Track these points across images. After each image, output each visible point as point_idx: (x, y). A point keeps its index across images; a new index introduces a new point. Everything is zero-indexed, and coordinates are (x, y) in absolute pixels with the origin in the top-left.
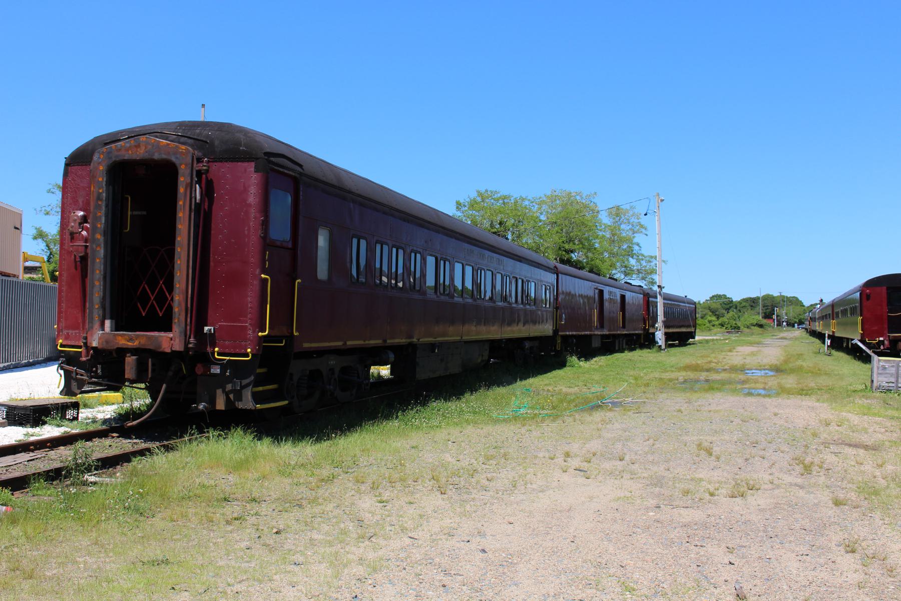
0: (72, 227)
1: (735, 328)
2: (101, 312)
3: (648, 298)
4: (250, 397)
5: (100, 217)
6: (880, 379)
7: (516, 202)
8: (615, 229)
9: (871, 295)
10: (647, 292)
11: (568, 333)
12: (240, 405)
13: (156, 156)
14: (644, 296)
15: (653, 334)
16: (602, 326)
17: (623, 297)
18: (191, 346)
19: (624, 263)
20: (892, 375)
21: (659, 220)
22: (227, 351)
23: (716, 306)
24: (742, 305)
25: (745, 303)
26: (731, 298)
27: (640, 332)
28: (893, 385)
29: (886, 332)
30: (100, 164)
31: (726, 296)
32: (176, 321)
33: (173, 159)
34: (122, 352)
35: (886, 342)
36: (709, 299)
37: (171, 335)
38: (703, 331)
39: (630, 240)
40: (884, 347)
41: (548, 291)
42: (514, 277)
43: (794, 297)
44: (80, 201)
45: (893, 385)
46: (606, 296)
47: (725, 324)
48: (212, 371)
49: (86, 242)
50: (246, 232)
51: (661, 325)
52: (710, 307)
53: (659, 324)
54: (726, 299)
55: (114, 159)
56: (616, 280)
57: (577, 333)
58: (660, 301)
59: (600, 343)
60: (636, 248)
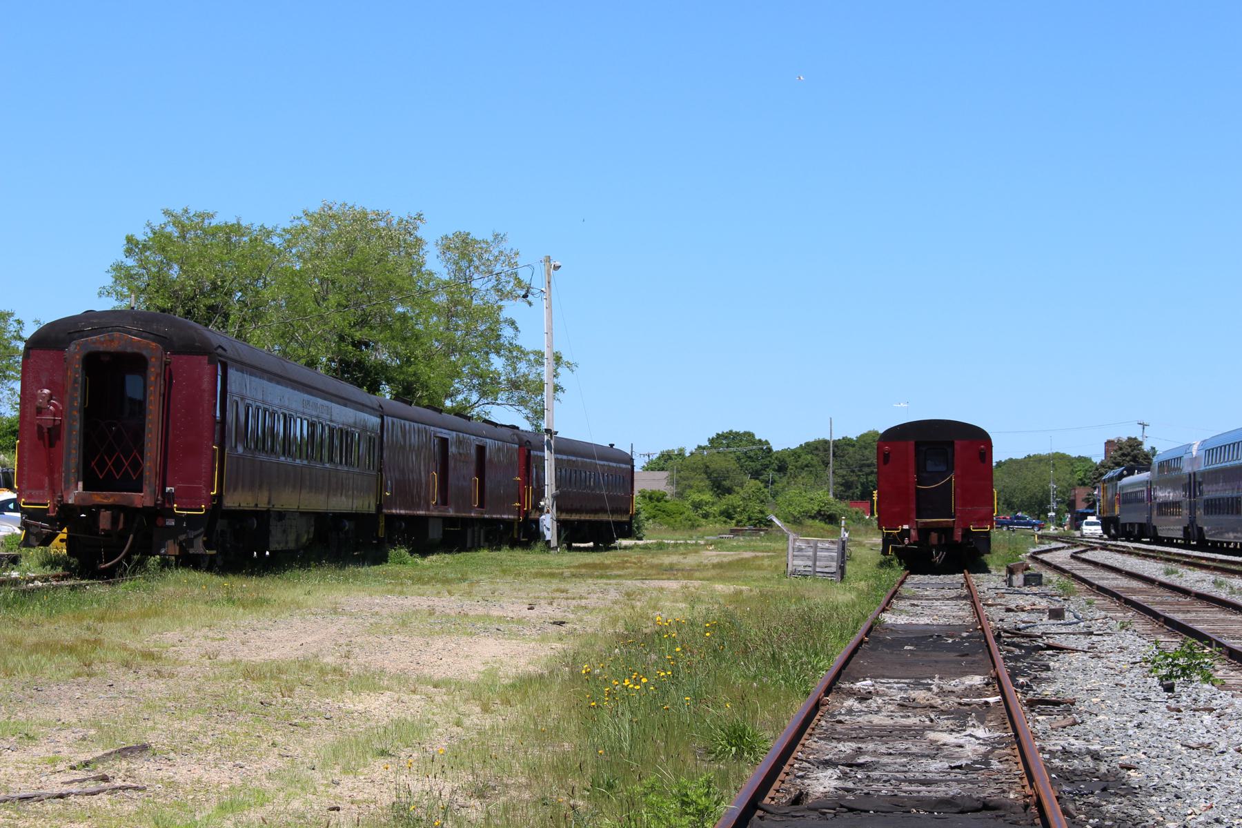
0: (41, 403)
1: (760, 522)
2: (76, 476)
3: (529, 451)
4: (201, 544)
5: (76, 397)
6: (796, 562)
7: (254, 241)
8: (460, 287)
9: (891, 455)
10: (525, 439)
11: (394, 511)
12: (191, 551)
13: (129, 350)
14: (520, 446)
15: (537, 522)
16: (444, 501)
17: (481, 450)
18: (159, 502)
19: (478, 368)
20: (808, 557)
21: (549, 307)
22: (184, 507)
23: (724, 464)
24: (802, 461)
25: (809, 457)
26: (767, 443)
27: (511, 517)
28: (810, 569)
29: (913, 515)
30: (75, 351)
31: (753, 435)
32: (147, 482)
33: (145, 353)
34: (100, 507)
35: (913, 533)
36: (706, 443)
37: (142, 494)
38: (674, 529)
39: (491, 314)
40: (909, 540)
42: (282, 413)
44: (44, 380)
45: (810, 569)
46: (452, 450)
47: (736, 512)
48: (167, 523)
49: (55, 416)
50: (201, 412)
51: (551, 502)
52: (707, 467)
53: (547, 502)
54: (754, 444)
55: (89, 350)
56: (469, 418)
57: (407, 512)
58: (549, 459)
59: (441, 532)
60: (507, 332)
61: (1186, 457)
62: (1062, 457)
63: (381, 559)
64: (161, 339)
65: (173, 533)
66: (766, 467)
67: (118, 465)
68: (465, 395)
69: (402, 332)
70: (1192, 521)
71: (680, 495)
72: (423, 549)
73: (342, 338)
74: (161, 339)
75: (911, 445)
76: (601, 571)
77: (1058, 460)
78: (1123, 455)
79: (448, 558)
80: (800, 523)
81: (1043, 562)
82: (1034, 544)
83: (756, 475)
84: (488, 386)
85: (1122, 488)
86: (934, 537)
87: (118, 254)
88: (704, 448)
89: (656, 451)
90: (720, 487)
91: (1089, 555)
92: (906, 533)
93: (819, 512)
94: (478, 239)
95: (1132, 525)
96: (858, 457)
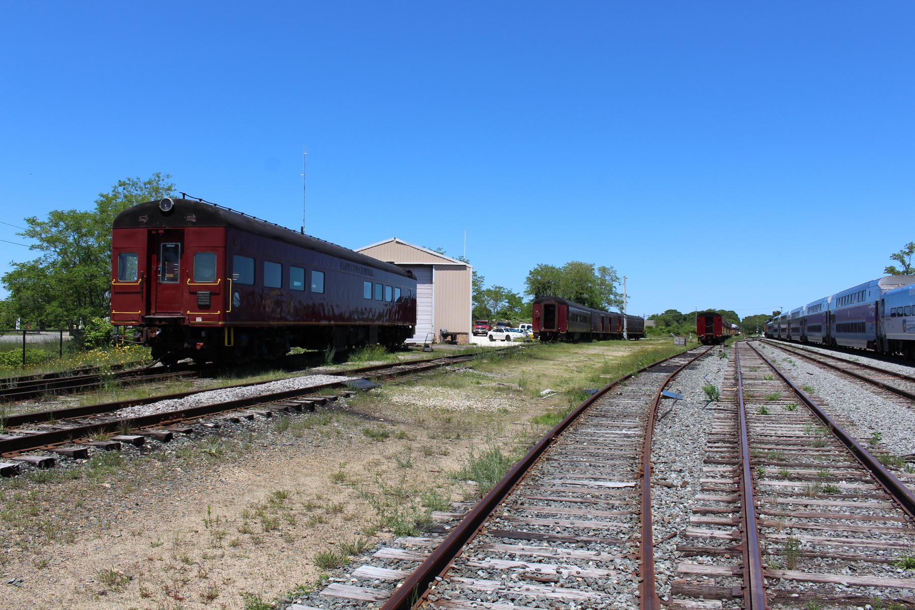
30: (543, 304)
41: (796, 351)
43: (732, 311)
53: (625, 330)
58: (625, 320)
60: (614, 289)
62: (764, 315)
63: (591, 342)
64: (557, 302)
66: (680, 319)
68: (605, 305)
69: (591, 290)
70: (803, 335)
71: (657, 327)
72: (599, 340)
73: (577, 292)
74: (557, 302)
76: (637, 344)
79: (604, 342)
83: (677, 321)
84: (610, 302)
86: (709, 338)
87: (528, 275)
89: (651, 315)
90: (667, 325)
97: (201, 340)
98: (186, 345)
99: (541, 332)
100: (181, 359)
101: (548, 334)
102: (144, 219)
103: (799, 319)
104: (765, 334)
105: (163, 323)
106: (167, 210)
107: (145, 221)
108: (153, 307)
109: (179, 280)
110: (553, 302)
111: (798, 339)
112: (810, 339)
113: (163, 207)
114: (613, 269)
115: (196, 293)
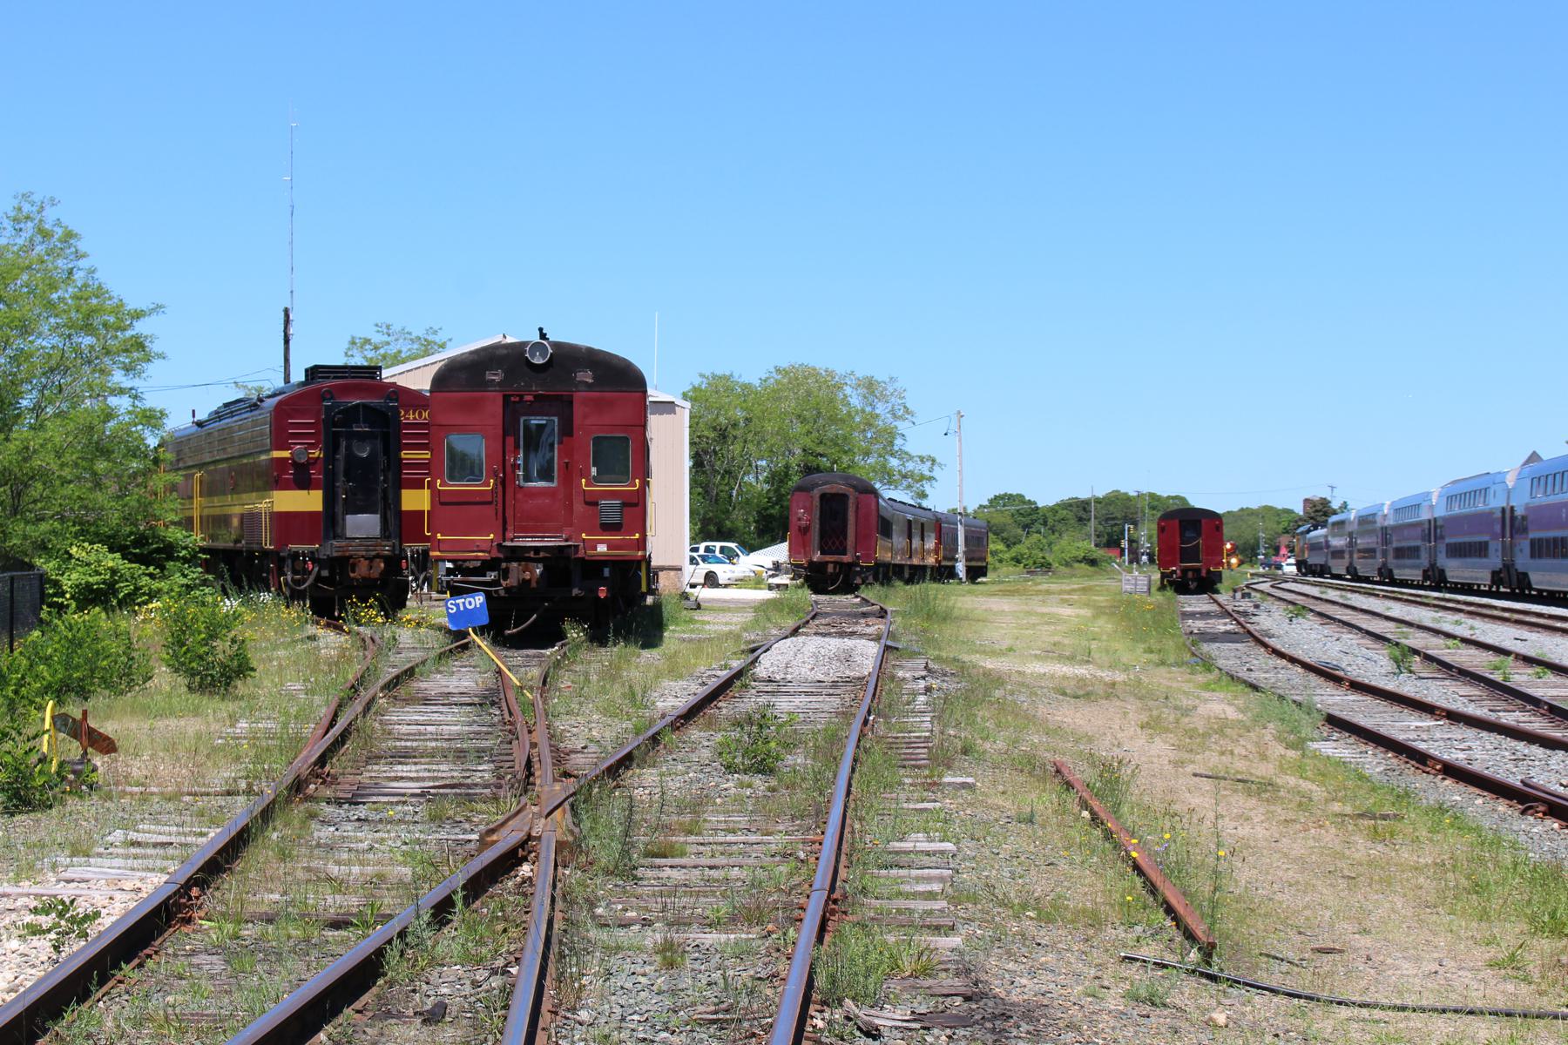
1: (1043, 566)
21: (960, 441)
23: (1003, 520)
25: (1065, 512)
30: (816, 493)
31: (1023, 496)
34: (827, 563)
35: (1178, 572)
43: (1176, 497)
53: (960, 555)
60: (898, 442)
61: (1380, 513)
64: (854, 487)
65: (859, 573)
66: (1033, 522)
67: (834, 543)
70: (1508, 567)
74: (854, 487)
75: (1177, 521)
77: (1268, 512)
78: (1317, 511)
80: (1071, 566)
81: (1252, 588)
82: (1247, 580)
84: (889, 477)
85: (1310, 539)
86: (1190, 574)
88: (985, 507)
91: (1283, 585)
92: (1174, 572)
93: (1084, 558)
94: (880, 380)
95: (1316, 565)
96: (1104, 512)
97: (604, 581)
98: (575, 591)
99: (811, 563)
100: (535, 620)
101: (830, 569)
102: (495, 376)
103: (1419, 524)
104: (1299, 564)
105: (542, 554)
106: (538, 361)
107: (497, 379)
108: (510, 528)
109: (556, 481)
110: (841, 488)
111: (1415, 575)
112: (1398, 574)
113: (533, 356)
114: (896, 385)
115: (596, 504)
